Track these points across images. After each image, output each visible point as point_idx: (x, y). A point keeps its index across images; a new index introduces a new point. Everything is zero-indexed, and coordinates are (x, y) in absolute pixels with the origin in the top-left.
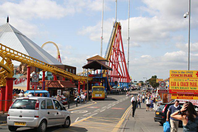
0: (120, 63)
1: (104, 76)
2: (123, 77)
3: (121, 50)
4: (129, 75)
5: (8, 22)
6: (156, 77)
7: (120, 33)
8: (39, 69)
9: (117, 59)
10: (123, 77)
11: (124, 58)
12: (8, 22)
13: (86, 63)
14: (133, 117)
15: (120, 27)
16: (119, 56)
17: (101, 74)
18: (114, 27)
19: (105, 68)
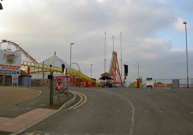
0: (117, 75)
1: (110, 83)
2: (119, 83)
3: (117, 68)
4: (25, 113)
5: (55, 54)
6: (178, 80)
7: (116, 57)
8: (28, 86)
9: (115, 72)
10: (119, 83)
11: (119, 72)
12: (55, 54)
13: (101, 77)
14: (115, 54)
15: (116, 55)
16: (116, 71)
17: (109, 82)
18: (113, 54)
19: (110, 79)
